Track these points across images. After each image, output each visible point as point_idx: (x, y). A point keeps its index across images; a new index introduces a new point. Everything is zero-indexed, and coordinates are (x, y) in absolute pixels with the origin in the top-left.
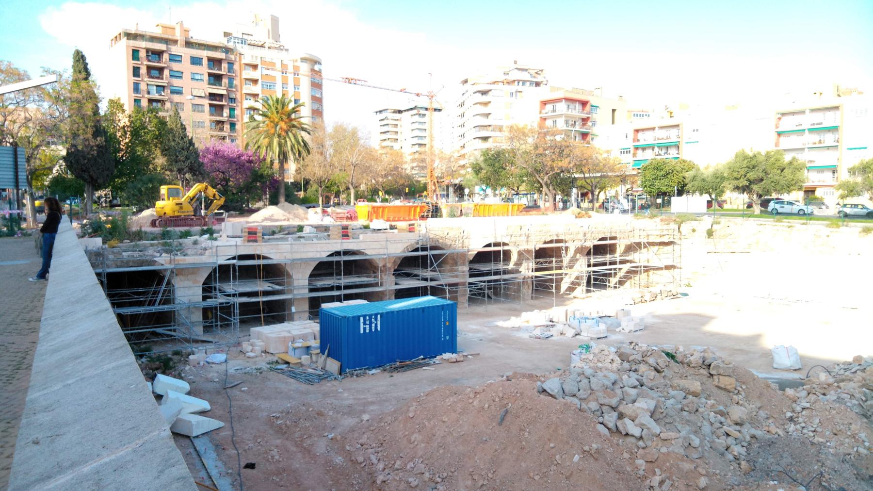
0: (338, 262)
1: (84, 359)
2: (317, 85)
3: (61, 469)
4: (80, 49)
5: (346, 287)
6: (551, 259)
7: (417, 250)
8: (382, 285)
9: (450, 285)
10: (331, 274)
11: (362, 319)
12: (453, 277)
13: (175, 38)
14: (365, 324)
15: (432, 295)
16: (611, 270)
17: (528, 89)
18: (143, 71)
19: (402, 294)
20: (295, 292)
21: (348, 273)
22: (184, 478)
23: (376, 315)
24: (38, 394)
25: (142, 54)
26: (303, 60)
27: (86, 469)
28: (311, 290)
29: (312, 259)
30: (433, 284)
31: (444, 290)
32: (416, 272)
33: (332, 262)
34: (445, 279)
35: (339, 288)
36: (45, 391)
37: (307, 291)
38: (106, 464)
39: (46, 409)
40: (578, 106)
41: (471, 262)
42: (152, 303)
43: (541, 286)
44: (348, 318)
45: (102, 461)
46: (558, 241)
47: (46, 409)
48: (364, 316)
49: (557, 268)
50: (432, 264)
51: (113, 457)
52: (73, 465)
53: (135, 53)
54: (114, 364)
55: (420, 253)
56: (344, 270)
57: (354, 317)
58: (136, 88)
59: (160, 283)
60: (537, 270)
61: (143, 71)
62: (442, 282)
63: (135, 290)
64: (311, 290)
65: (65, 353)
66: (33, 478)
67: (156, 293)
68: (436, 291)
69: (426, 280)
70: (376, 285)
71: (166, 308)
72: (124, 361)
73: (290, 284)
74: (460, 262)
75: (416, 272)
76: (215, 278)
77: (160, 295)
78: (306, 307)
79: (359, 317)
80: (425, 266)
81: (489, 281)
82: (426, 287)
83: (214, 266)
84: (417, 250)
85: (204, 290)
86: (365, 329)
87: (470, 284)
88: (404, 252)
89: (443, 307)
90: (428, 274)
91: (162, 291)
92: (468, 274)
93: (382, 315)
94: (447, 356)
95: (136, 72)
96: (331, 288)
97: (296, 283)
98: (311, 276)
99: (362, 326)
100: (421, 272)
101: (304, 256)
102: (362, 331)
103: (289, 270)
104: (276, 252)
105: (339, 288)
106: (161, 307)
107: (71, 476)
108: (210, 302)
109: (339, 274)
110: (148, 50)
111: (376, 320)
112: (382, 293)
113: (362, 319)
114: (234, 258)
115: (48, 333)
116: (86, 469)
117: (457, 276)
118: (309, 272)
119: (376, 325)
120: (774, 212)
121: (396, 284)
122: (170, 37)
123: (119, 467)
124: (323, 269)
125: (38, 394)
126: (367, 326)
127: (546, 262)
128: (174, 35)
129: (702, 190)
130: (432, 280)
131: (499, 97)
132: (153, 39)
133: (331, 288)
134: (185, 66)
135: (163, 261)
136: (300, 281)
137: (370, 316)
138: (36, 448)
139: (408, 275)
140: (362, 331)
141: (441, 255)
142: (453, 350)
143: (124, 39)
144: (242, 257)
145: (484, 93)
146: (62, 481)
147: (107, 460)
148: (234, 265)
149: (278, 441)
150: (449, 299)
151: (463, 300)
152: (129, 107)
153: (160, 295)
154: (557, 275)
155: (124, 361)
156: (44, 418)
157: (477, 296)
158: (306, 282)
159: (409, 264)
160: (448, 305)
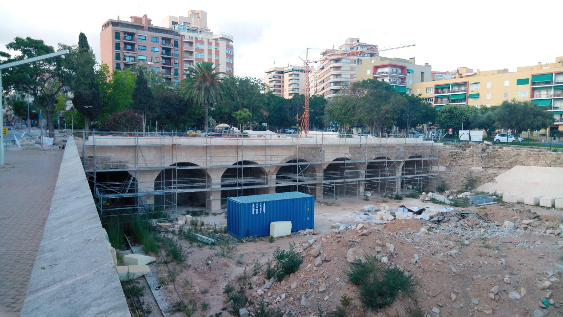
0: (240, 169)
1: (73, 224)
2: (230, 56)
3: (55, 282)
4: (83, 32)
5: (245, 185)
6: (377, 170)
7: (290, 162)
8: (267, 183)
9: (311, 185)
10: (235, 176)
11: (253, 205)
12: (313, 179)
13: (142, 25)
14: (255, 208)
15: (299, 191)
16: (417, 177)
17: (365, 59)
18: (122, 46)
19: (279, 190)
20: (213, 187)
21: (246, 176)
22: (117, 288)
23: (263, 203)
24: (46, 242)
25: (122, 35)
26: (222, 39)
27: (68, 283)
28: (222, 186)
29: (223, 167)
30: (300, 184)
31: (307, 188)
32: (289, 176)
33: (236, 168)
34: (307, 181)
35: (240, 185)
36: (50, 241)
37: (220, 186)
38: (79, 280)
39: (50, 250)
40: (399, 71)
41: (325, 170)
42: (124, 192)
43: (371, 187)
44: (245, 204)
45: (77, 278)
46: (418, 157)
47: (50, 250)
48: (255, 204)
49: (381, 176)
50: (300, 171)
51: (82, 277)
52: (61, 280)
53: (117, 35)
54: (89, 227)
55: (292, 164)
56: (244, 174)
57: (248, 204)
58: (118, 57)
59: (129, 180)
60: (368, 176)
61: (122, 46)
62: (306, 183)
63: (114, 183)
64: (222, 186)
65: (63, 220)
66: (40, 287)
67: (127, 185)
68: (302, 189)
69: (296, 181)
70: (264, 184)
71: (132, 195)
72: (95, 225)
73: (209, 181)
74: (317, 170)
75: (289, 176)
76: (163, 177)
77: (129, 187)
78: (219, 196)
79: (252, 204)
80: (295, 172)
81: (336, 183)
82: (295, 186)
83: (162, 169)
84: (290, 162)
85: (156, 185)
86: (255, 211)
87: (324, 184)
88: (281, 163)
89: (305, 199)
90: (297, 177)
91: (130, 184)
92: (323, 178)
93: (266, 202)
94: (308, 230)
95: (117, 46)
96: (235, 185)
97: (213, 181)
98: (223, 177)
99: (253, 209)
100: (292, 176)
101: (218, 164)
102: (253, 213)
103: (209, 173)
104: (201, 163)
105: (240, 185)
106: (129, 194)
107: (60, 286)
108: (159, 192)
109: (240, 176)
110: (125, 33)
111: (263, 206)
112: (268, 188)
113: (253, 205)
114: (175, 165)
115: (55, 208)
116: (68, 283)
117: (315, 179)
118: (221, 175)
119: (263, 209)
120: (498, 141)
121: (277, 183)
122: (139, 25)
123: (85, 282)
124: (230, 173)
125: (46, 242)
126: (257, 210)
127: (374, 171)
128: (141, 23)
129: (480, 127)
130: (299, 181)
131: (346, 63)
132: (128, 25)
133: (235, 185)
134: (148, 43)
135: (130, 167)
136: (216, 179)
137: (259, 203)
138: (43, 271)
139: (284, 178)
140: (253, 213)
141: (306, 166)
142: (312, 227)
143: (111, 26)
144: (180, 164)
145: (337, 61)
146: (54, 288)
147: (79, 278)
148: (175, 169)
149: (199, 281)
150: (310, 194)
151: (319, 193)
152: (111, 69)
153: (129, 187)
154: (381, 180)
155: (95, 225)
156: (48, 255)
157: (329, 191)
158: (220, 181)
159: (284, 171)
160: (309, 197)
